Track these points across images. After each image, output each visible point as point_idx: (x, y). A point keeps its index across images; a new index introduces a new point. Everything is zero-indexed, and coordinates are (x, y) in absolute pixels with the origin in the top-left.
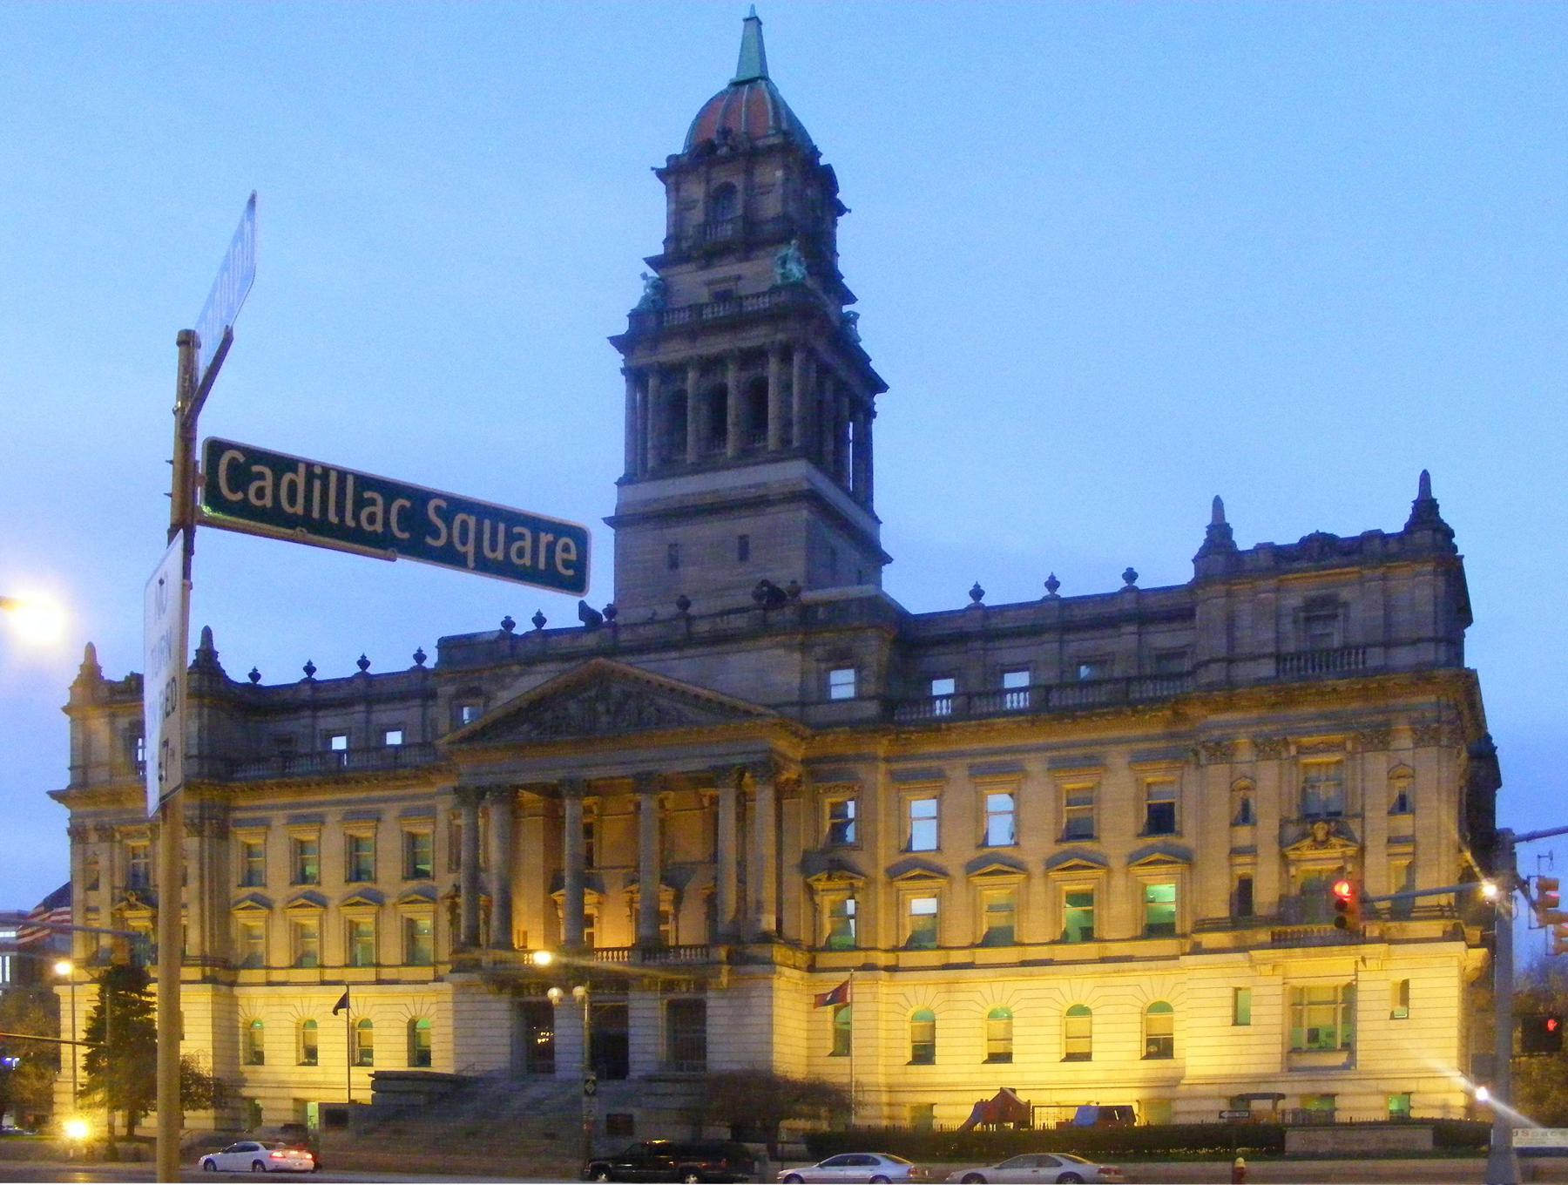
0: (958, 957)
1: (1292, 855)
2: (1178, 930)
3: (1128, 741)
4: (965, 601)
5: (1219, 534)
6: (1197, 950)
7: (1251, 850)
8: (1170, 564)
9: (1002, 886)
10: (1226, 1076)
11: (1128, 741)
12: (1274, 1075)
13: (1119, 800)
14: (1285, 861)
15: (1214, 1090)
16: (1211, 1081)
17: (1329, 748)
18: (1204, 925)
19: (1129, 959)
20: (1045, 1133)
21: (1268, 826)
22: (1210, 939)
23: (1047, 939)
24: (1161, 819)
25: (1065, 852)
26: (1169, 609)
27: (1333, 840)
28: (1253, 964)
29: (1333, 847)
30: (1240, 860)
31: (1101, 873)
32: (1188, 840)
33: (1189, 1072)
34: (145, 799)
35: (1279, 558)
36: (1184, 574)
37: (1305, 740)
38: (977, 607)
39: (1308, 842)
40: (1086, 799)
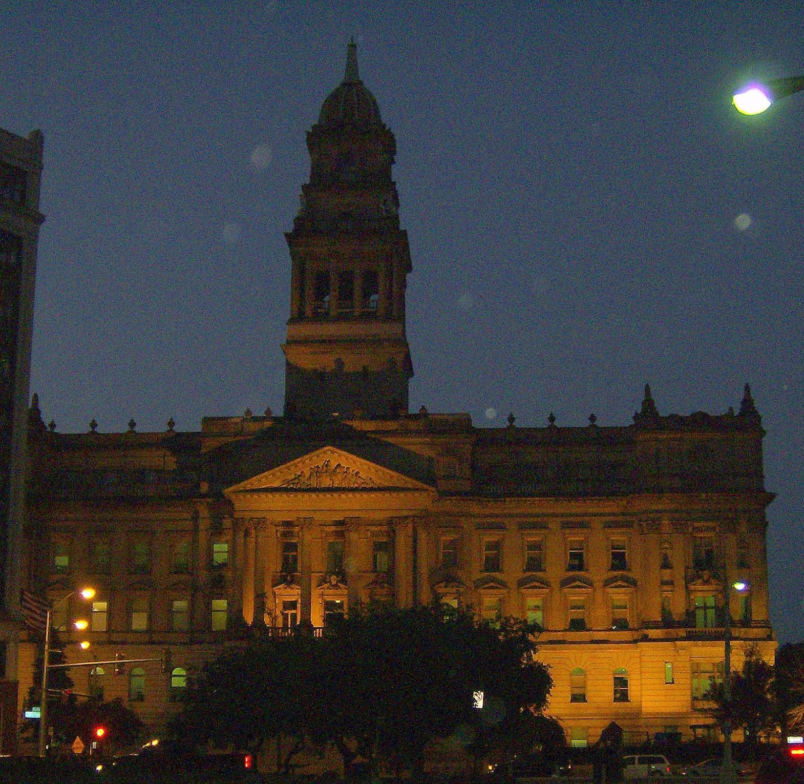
0: (559, 636)
1: (692, 587)
2: (631, 626)
3: (602, 515)
4: (125, 429)
5: (649, 403)
6: (646, 639)
7: (671, 583)
8: (620, 414)
9: (536, 595)
10: (670, 713)
11: (602, 515)
12: (684, 714)
13: (598, 547)
14: (689, 592)
15: (659, 721)
16: (656, 716)
17: (708, 529)
18: (647, 625)
19: (563, 642)
20: (578, 750)
21: (679, 572)
22: (653, 633)
23: (605, 627)
24: (619, 560)
25: (527, 578)
26: (609, 438)
27: (713, 581)
28: (676, 650)
29: (711, 584)
30: (665, 588)
31: (505, 591)
32: (634, 574)
33: (644, 710)
34: (362, 418)
35: (677, 422)
36: (627, 421)
37: (696, 524)
38: (93, 433)
39: (700, 581)
40: (496, 546)
